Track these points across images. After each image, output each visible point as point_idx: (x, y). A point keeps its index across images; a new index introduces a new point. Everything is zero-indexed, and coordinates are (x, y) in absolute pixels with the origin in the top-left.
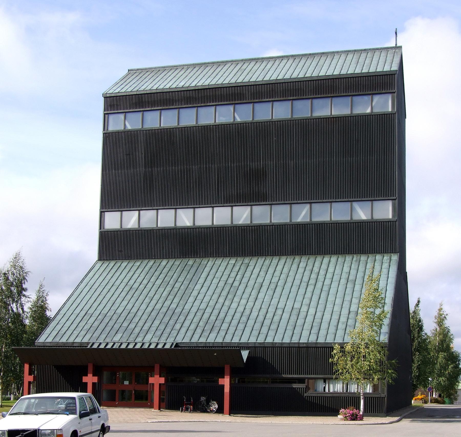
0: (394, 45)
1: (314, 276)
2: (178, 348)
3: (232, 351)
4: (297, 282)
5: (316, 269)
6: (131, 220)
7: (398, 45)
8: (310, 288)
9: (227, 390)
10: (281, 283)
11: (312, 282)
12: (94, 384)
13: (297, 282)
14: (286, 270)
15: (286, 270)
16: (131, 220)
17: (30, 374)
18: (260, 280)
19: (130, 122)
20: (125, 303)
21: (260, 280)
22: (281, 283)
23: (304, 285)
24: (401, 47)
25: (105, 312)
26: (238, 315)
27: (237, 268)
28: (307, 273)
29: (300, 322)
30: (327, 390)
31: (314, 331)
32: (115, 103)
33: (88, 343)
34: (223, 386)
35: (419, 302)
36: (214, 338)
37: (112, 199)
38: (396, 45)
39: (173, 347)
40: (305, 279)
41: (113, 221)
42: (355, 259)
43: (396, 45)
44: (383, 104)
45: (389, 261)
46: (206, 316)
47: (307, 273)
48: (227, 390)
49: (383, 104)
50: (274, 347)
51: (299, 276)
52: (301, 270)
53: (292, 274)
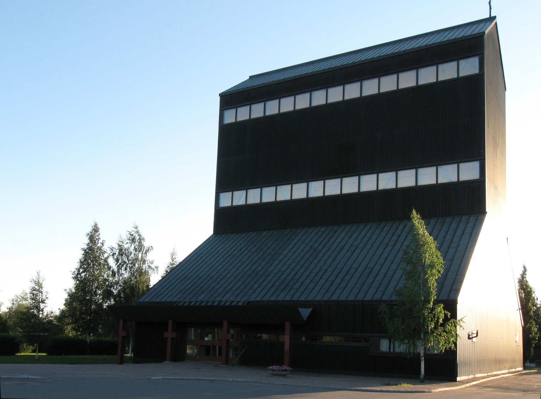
0: (488, 16)
1: (395, 238)
2: (251, 306)
3: (293, 306)
4: (377, 244)
5: (398, 232)
6: (240, 198)
7: (492, 16)
8: (388, 249)
9: (287, 347)
10: (361, 246)
11: (392, 243)
12: (172, 339)
13: (377, 244)
14: (369, 234)
15: (369, 234)
16: (240, 198)
17: (123, 330)
18: (343, 243)
19: (243, 114)
20: (220, 267)
21: (343, 243)
22: (361, 246)
23: (383, 246)
24: (495, 18)
25: (201, 275)
26: (313, 275)
27: (325, 235)
28: (389, 235)
29: (370, 280)
30: (392, 350)
31: (382, 288)
32: (230, 100)
33: (176, 302)
34: (283, 343)
35: (524, 267)
36: (284, 296)
37: (226, 181)
38: (490, 15)
39: (245, 304)
40: (386, 241)
41: (226, 201)
42: (440, 221)
43: (490, 15)
44: (468, 67)
45: (475, 220)
46: (284, 276)
47: (389, 235)
48: (287, 347)
49: (468, 67)
50: (338, 303)
51: (380, 239)
52: (384, 233)
53: (374, 237)
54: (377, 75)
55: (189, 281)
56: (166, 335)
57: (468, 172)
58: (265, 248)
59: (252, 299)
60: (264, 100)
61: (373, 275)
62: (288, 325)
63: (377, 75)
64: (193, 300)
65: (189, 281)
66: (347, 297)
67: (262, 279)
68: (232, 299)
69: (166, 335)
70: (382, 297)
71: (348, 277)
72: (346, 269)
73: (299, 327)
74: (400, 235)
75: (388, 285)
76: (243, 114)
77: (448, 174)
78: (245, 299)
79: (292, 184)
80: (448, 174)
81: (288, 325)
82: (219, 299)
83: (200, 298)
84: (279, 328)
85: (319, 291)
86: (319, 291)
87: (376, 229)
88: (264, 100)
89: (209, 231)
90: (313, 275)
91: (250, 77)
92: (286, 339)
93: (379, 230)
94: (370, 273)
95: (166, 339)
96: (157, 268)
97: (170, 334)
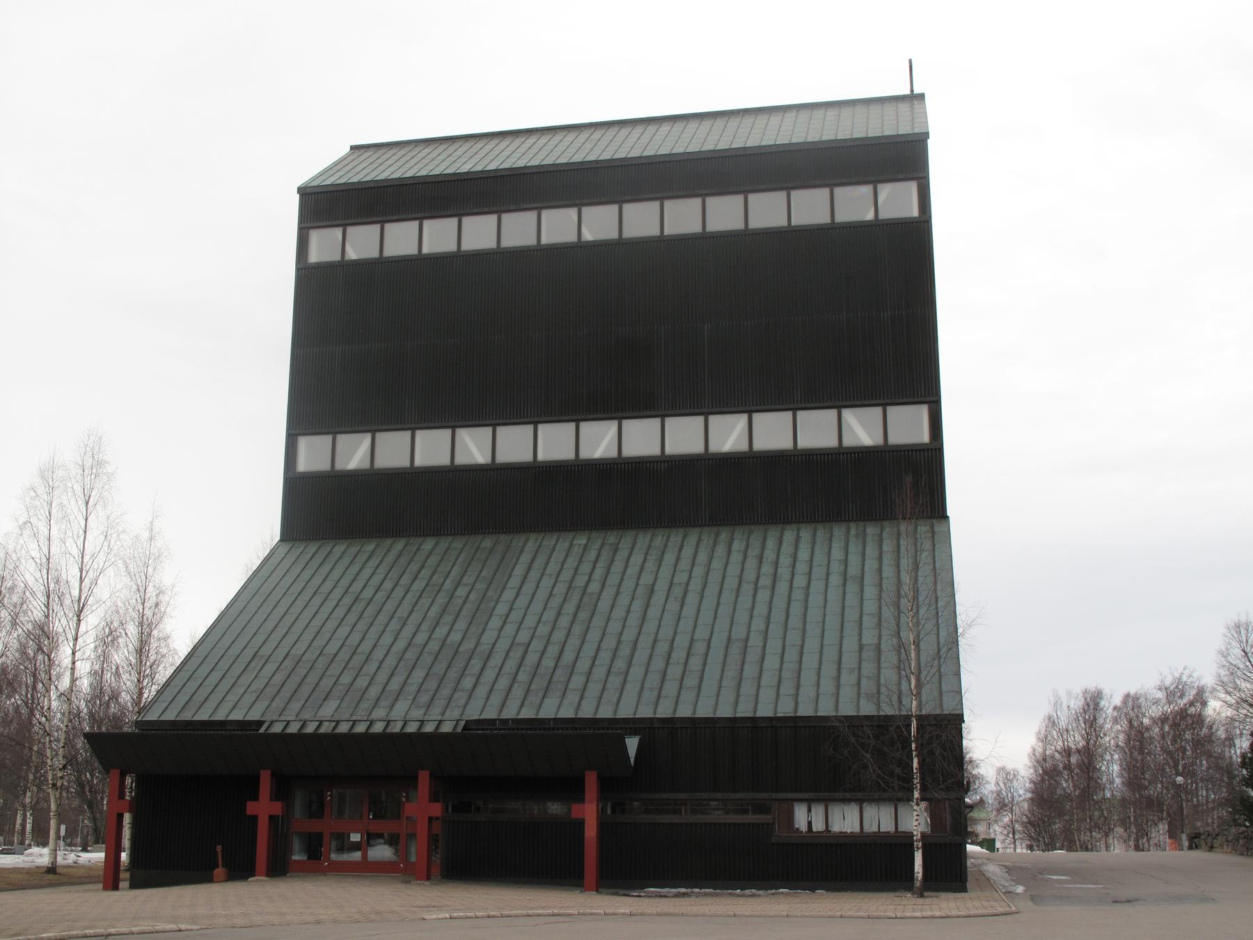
2: (480, 735)
6: (355, 453)
8: (763, 596)
16: (355, 453)
19: (362, 242)
26: (605, 656)
29: (750, 670)
32: (324, 205)
33: (259, 723)
34: (580, 824)
43: (912, 90)
46: (532, 659)
54: (700, 192)
55: (270, 668)
56: (251, 808)
57: (907, 426)
58: (448, 585)
59: (473, 713)
60: (420, 215)
61: (753, 656)
62: (591, 780)
63: (700, 192)
64: (306, 715)
65: (270, 668)
66: (501, 711)
67: (476, 664)
68: (417, 714)
69: (251, 808)
70: (675, 710)
71: (695, 663)
72: (682, 641)
73: (619, 784)
74: (776, 564)
75: (799, 682)
76: (362, 242)
77: (861, 428)
78: (454, 713)
79: (494, 426)
80: (861, 428)
81: (591, 780)
82: (380, 713)
83: (328, 710)
84: (572, 789)
85: (639, 697)
86: (639, 697)
87: (715, 545)
88: (420, 215)
89: (278, 538)
90: (605, 656)
91: (352, 148)
92: (589, 813)
93: (721, 550)
94: (744, 653)
95: (255, 818)
96: (184, 629)
97: (263, 808)
